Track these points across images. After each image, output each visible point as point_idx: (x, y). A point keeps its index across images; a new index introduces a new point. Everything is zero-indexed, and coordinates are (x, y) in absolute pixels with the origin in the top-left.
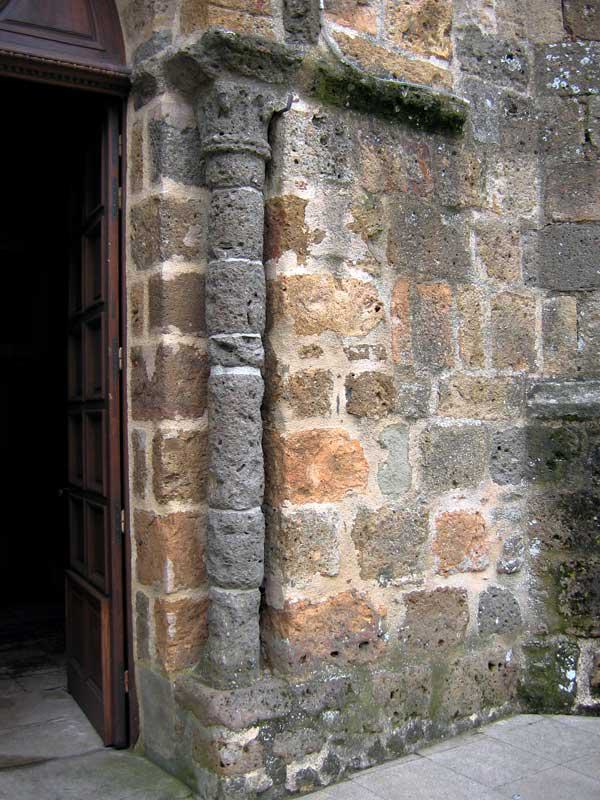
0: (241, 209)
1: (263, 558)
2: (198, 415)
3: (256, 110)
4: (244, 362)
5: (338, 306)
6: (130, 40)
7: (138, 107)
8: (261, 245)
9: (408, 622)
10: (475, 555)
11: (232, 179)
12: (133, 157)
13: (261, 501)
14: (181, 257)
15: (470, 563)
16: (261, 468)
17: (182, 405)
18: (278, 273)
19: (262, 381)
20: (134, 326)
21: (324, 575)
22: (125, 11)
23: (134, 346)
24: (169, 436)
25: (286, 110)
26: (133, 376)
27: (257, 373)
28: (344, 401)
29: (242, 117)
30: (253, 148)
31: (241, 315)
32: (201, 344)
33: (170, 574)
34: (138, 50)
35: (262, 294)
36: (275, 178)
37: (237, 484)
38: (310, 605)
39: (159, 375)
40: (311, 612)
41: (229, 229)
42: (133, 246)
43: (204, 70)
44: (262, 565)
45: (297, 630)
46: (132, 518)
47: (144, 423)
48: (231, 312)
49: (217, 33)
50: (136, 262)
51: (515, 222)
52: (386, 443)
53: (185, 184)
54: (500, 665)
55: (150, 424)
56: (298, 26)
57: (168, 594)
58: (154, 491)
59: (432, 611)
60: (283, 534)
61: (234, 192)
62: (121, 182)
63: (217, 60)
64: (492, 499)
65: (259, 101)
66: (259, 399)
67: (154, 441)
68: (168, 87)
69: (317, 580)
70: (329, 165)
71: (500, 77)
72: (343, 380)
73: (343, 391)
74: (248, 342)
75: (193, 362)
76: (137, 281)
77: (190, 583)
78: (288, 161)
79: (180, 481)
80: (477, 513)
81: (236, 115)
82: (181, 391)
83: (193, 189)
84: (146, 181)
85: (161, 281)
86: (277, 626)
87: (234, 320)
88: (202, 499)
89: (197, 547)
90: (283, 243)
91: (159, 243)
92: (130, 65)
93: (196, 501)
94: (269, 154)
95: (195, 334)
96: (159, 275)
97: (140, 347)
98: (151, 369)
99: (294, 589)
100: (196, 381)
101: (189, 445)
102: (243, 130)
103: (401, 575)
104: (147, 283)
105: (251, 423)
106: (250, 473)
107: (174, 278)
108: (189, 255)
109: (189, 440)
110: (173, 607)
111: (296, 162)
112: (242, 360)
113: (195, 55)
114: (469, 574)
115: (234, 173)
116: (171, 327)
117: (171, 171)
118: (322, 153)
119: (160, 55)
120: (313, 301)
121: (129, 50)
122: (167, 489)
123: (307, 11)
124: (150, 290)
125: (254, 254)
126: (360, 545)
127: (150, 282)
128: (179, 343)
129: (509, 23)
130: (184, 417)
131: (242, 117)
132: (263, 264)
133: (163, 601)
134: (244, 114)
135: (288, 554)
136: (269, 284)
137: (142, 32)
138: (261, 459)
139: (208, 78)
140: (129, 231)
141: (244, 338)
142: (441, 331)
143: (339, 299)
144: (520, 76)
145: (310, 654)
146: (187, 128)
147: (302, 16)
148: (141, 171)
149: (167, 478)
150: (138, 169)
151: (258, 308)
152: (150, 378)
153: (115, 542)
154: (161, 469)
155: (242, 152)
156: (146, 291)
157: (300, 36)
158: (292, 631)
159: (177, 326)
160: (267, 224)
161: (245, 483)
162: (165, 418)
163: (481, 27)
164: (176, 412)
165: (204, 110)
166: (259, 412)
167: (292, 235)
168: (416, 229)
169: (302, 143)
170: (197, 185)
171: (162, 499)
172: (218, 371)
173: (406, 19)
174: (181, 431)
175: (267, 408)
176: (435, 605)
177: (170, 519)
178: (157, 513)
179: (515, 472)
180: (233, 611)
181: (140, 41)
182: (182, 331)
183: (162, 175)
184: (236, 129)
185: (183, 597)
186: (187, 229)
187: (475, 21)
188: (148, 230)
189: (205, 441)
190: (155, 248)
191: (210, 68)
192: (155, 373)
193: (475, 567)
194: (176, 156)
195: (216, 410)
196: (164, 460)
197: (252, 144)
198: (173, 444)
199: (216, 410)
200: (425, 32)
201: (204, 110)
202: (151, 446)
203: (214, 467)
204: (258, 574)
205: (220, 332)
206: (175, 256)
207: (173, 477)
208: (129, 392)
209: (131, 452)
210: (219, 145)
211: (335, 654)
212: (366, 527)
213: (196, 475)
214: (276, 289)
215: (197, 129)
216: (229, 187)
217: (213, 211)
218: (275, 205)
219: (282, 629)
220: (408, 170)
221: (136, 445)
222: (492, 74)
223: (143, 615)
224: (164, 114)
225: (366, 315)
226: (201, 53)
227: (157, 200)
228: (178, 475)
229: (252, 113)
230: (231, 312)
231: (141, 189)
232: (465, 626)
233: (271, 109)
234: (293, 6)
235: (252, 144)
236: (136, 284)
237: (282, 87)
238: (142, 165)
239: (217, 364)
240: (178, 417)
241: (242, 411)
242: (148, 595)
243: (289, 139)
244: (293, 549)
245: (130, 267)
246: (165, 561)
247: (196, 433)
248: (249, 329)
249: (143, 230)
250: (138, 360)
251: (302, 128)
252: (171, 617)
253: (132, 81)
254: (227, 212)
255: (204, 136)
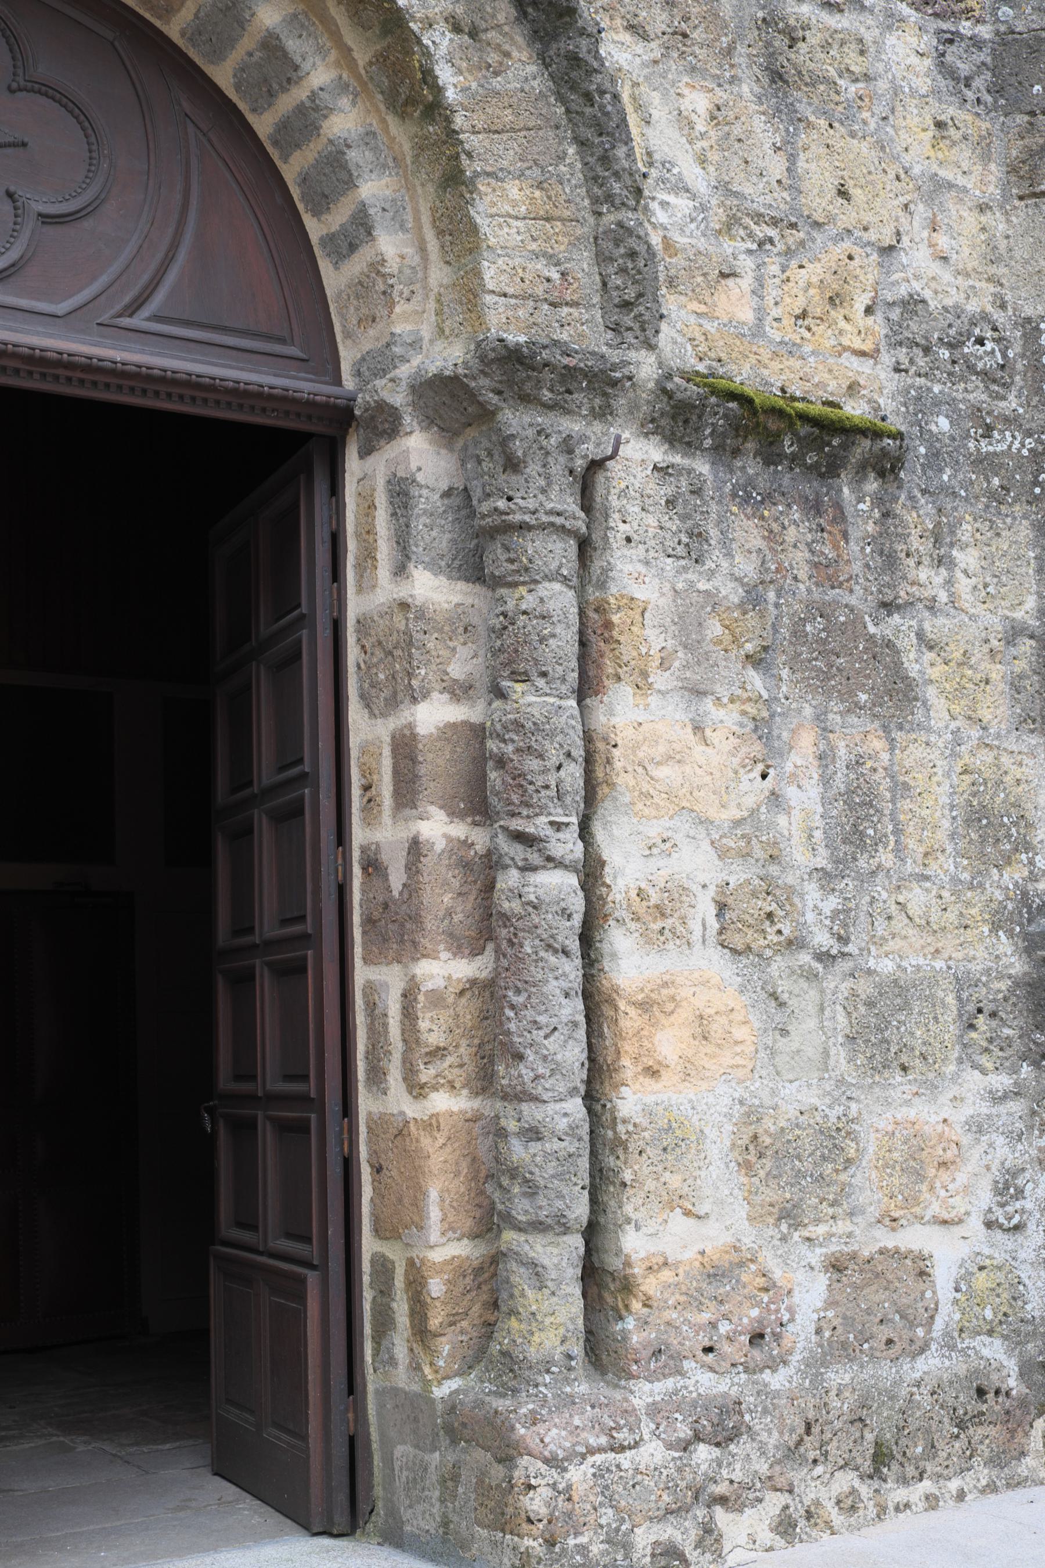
0: (544, 618)
1: (587, 1182)
2: (476, 952)
3: (562, 459)
4: (552, 862)
5: (699, 771)
6: (349, 342)
7: (365, 452)
8: (576, 675)
9: (831, 1303)
10: (943, 1193)
11: (527, 570)
12: (358, 535)
13: (582, 1089)
14: (446, 696)
15: (935, 1209)
16: (581, 1033)
17: (451, 935)
18: (603, 719)
19: (581, 894)
20: (363, 810)
21: (687, 1213)
22: (339, 295)
23: (366, 842)
24: (429, 985)
25: (611, 458)
26: (363, 892)
27: (572, 880)
28: (714, 925)
29: (541, 470)
30: (559, 520)
31: (547, 787)
32: (480, 838)
33: (434, 1214)
34: (363, 359)
35: (579, 753)
36: (597, 566)
37: (545, 1058)
38: (666, 1264)
39: (411, 889)
40: (666, 1275)
41: (526, 652)
42: (361, 680)
43: (481, 399)
44: (586, 1193)
45: (645, 1305)
46: (363, 1129)
47: (384, 969)
48: (531, 783)
49: (501, 340)
50: (368, 706)
51: (995, 622)
52: (785, 997)
53: (450, 578)
54: (997, 1392)
55: (396, 968)
56: (628, 320)
57: (431, 1247)
58: (405, 1079)
59: (874, 1288)
60: (619, 1144)
61: (530, 591)
62: (337, 574)
63: (501, 382)
64: (970, 1098)
65: (568, 446)
66: (577, 920)
67: (404, 995)
68: (419, 423)
69: (678, 1222)
70: (679, 543)
71: (963, 379)
72: (712, 891)
73: (713, 911)
74: (558, 830)
75: (466, 865)
76: (370, 737)
77: (466, 1229)
78: (616, 540)
79: (450, 1060)
80: (945, 1121)
81: (533, 469)
82: (449, 913)
83: (461, 585)
84: (384, 572)
85: (414, 736)
86: (610, 1300)
87: (535, 795)
88: (484, 1090)
89: (478, 1171)
90: (610, 671)
91: (410, 675)
92: (349, 383)
93: (476, 1094)
94: (584, 529)
95: (469, 820)
96: (411, 726)
97: (377, 844)
98: (397, 879)
99: (640, 1233)
100: (472, 898)
101: (463, 1001)
102: (544, 491)
103: (818, 1221)
104: (388, 740)
105: (564, 959)
106: (565, 1041)
107: (434, 731)
108: (460, 691)
109: (462, 993)
110: (439, 1269)
111: (629, 540)
112: (549, 859)
113: (466, 376)
114: (937, 1227)
115: (530, 561)
116: (433, 810)
117: (427, 559)
118: (668, 525)
119: (404, 371)
120: (659, 763)
121: (347, 356)
122: (426, 1074)
123: (641, 295)
124: (393, 751)
125: (564, 689)
126: (747, 1167)
127: (393, 737)
128: (445, 835)
129: (978, 284)
130: (455, 955)
131: (541, 470)
132: (579, 703)
133: (422, 1261)
134: (544, 466)
135: (627, 1176)
136: (588, 737)
137: (371, 332)
138: (581, 1019)
139: (485, 410)
140: (353, 654)
141: (551, 823)
142: (872, 812)
143: (702, 760)
144: (1000, 374)
145: (668, 1346)
146: (451, 489)
147: (632, 304)
148: (374, 559)
149: (427, 1054)
150: (369, 555)
151: (573, 774)
152: (396, 894)
153: (335, 1171)
154: (417, 1041)
155: (543, 527)
156: (387, 751)
157: (629, 337)
158: (636, 1305)
159: (441, 808)
160: (583, 643)
161: (559, 1057)
162: (424, 956)
163: (927, 294)
164: (442, 947)
165: (479, 462)
166: (577, 943)
167: (625, 658)
168: (824, 642)
169: (637, 509)
170: (467, 580)
171: (417, 1090)
172: (509, 879)
173: (800, 294)
174: (449, 978)
175: (588, 938)
176: (877, 1276)
177: (431, 1124)
178: (410, 1114)
179: (1009, 1052)
180: (540, 1269)
181: (367, 346)
182: (448, 815)
183: (411, 565)
184: (532, 491)
185: (456, 1253)
186: (454, 649)
187: (916, 286)
188: (390, 653)
189: (487, 994)
190: (402, 681)
191: (491, 395)
192: (404, 885)
193: (946, 1216)
194: (434, 533)
195: (510, 941)
196: (423, 1025)
197: (559, 514)
198: (436, 999)
199: (510, 941)
200: (833, 313)
201: (479, 462)
202: (398, 1006)
203: (508, 1033)
204: (580, 1210)
205: (513, 815)
206: (435, 695)
207: (437, 1053)
208: (356, 918)
209: (360, 1019)
210: (504, 517)
211: (708, 1350)
212: (755, 1137)
213: (474, 1049)
214: (600, 746)
215: (466, 489)
216: (524, 583)
217: (498, 622)
218: (596, 610)
219: (621, 1305)
220: (808, 544)
221: (371, 1007)
222: (950, 374)
223: (385, 1291)
224: (413, 467)
225: (745, 786)
226: (475, 371)
227: (404, 606)
228: (445, 1049)
229: (558, 466)
230: (531, 783)
231: (374, 586)
232: (932, 1317)
233: (586, 456)
234: (617, 288)
235: (559, 514)
236: (367, 741)
237: (603, 413)
238: (376, 549)
239: (506, 867)
240: (444, 955)
241: (551, 941)
242: (391, 1256)
243: (614, 502)
244: (636, 1167)
245: (355, 713)
246: (425, 1194)
247: (473, 982)
248: (560, 811)
249: (379, 654)
250: (373, 866)
251: (637, 485)
252: (436, 1287)
253: (357, 412)
254: (520, 624)
255: (479, 501)
